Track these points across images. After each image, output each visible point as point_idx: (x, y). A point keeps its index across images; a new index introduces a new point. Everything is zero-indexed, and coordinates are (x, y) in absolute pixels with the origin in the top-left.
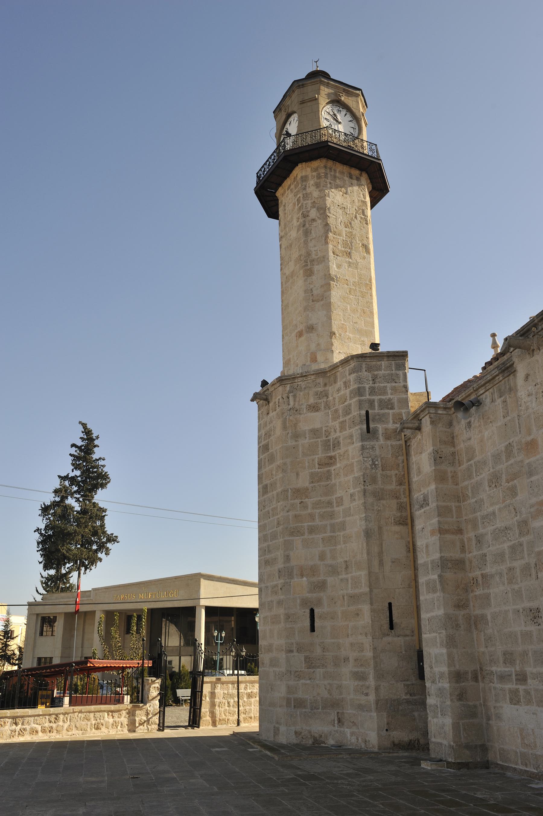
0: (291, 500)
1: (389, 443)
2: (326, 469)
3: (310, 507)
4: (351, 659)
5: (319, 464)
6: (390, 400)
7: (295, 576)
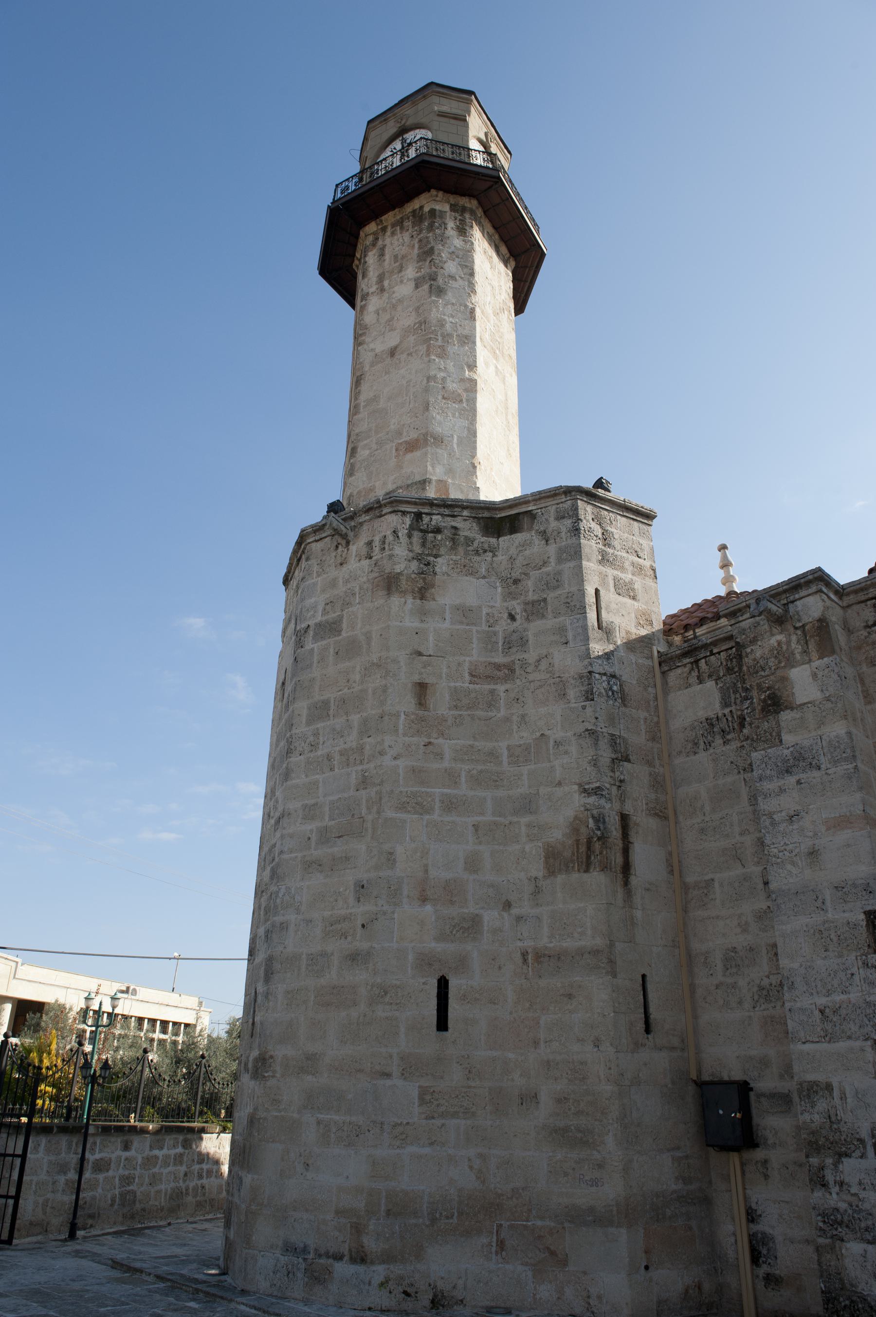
0: (405, 735)
1: (633, 657)
2: (487, 687)
3: (447, 756)
4: (543, 1097)
5: (471, 675)
6: (631, 582)
7: (405, 900)
